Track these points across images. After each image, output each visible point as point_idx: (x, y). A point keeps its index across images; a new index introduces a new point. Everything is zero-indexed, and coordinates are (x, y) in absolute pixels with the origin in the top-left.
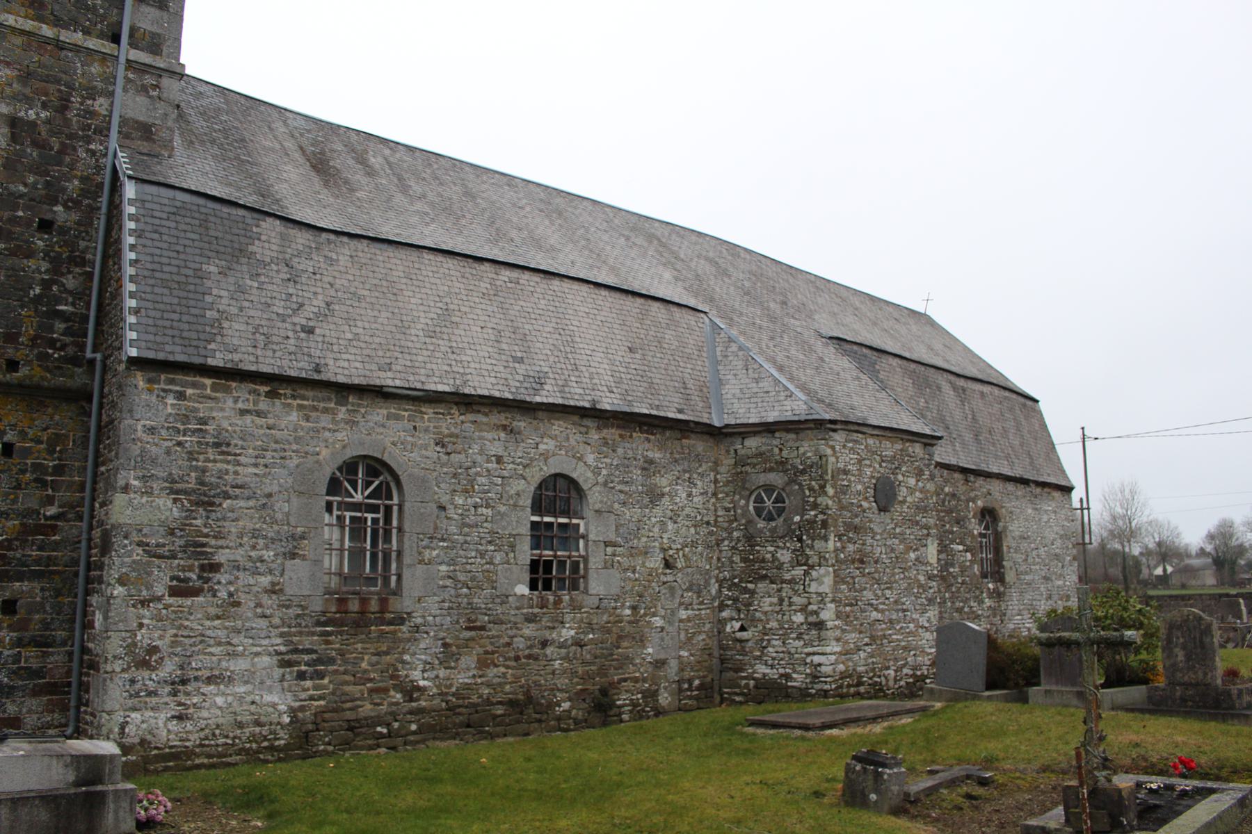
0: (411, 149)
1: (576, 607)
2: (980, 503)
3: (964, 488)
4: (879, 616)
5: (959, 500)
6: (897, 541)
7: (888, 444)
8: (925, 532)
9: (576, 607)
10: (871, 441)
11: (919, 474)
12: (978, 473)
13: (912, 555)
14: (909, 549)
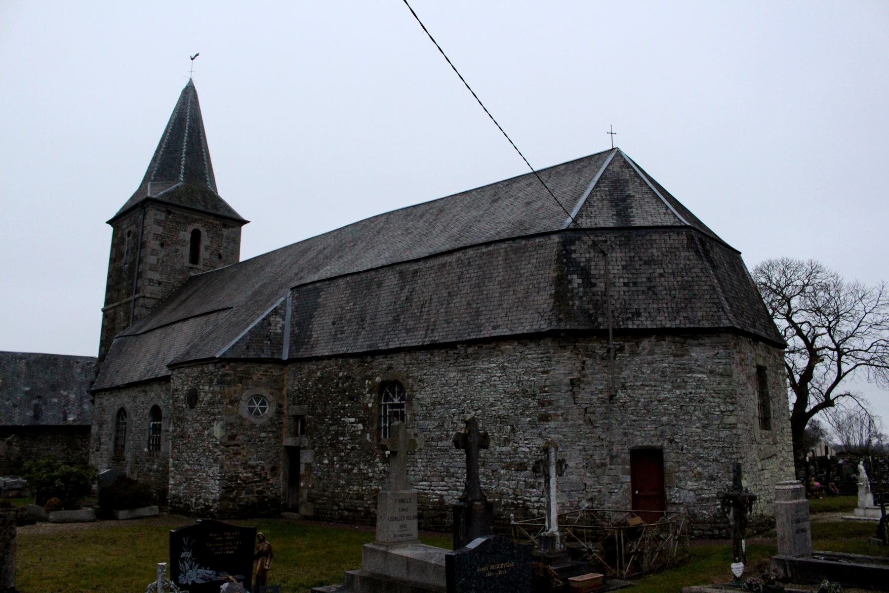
0: (402, 209)
1: (158, 457)
2: (378, 379)
3: (360, 370)
4: (189, 467)
5: (354, 380)
6: (198, 425)
7: (195, 369)
8: (212, 417)
9: (158, 457)
10: (187, 371)
11: (210, 382)
12: (375, 353)
13: (206, 432)
14: (204, 429)
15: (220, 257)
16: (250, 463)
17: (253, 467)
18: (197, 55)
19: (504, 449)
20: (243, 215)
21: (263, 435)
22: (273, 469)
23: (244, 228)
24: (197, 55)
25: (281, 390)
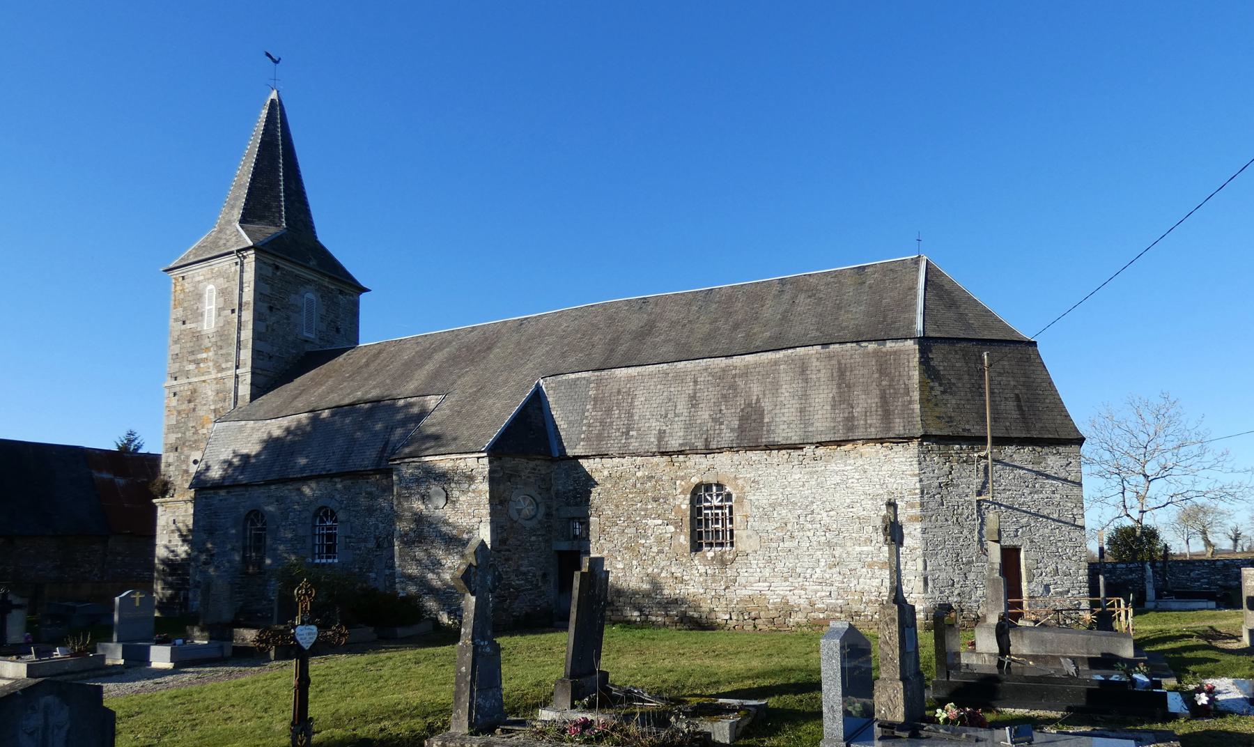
15: (338, 330)
16: (523, 569)
17: (524, 574)
18: (268, 55)
19: (865, 549)
20: (363, 282)
21: (533, 538)
22: (544, 575)
23: (363, 297)
24: (268, 55)
25: (548, 489)
